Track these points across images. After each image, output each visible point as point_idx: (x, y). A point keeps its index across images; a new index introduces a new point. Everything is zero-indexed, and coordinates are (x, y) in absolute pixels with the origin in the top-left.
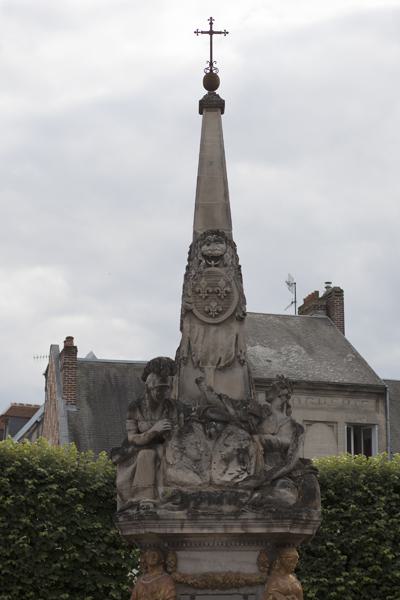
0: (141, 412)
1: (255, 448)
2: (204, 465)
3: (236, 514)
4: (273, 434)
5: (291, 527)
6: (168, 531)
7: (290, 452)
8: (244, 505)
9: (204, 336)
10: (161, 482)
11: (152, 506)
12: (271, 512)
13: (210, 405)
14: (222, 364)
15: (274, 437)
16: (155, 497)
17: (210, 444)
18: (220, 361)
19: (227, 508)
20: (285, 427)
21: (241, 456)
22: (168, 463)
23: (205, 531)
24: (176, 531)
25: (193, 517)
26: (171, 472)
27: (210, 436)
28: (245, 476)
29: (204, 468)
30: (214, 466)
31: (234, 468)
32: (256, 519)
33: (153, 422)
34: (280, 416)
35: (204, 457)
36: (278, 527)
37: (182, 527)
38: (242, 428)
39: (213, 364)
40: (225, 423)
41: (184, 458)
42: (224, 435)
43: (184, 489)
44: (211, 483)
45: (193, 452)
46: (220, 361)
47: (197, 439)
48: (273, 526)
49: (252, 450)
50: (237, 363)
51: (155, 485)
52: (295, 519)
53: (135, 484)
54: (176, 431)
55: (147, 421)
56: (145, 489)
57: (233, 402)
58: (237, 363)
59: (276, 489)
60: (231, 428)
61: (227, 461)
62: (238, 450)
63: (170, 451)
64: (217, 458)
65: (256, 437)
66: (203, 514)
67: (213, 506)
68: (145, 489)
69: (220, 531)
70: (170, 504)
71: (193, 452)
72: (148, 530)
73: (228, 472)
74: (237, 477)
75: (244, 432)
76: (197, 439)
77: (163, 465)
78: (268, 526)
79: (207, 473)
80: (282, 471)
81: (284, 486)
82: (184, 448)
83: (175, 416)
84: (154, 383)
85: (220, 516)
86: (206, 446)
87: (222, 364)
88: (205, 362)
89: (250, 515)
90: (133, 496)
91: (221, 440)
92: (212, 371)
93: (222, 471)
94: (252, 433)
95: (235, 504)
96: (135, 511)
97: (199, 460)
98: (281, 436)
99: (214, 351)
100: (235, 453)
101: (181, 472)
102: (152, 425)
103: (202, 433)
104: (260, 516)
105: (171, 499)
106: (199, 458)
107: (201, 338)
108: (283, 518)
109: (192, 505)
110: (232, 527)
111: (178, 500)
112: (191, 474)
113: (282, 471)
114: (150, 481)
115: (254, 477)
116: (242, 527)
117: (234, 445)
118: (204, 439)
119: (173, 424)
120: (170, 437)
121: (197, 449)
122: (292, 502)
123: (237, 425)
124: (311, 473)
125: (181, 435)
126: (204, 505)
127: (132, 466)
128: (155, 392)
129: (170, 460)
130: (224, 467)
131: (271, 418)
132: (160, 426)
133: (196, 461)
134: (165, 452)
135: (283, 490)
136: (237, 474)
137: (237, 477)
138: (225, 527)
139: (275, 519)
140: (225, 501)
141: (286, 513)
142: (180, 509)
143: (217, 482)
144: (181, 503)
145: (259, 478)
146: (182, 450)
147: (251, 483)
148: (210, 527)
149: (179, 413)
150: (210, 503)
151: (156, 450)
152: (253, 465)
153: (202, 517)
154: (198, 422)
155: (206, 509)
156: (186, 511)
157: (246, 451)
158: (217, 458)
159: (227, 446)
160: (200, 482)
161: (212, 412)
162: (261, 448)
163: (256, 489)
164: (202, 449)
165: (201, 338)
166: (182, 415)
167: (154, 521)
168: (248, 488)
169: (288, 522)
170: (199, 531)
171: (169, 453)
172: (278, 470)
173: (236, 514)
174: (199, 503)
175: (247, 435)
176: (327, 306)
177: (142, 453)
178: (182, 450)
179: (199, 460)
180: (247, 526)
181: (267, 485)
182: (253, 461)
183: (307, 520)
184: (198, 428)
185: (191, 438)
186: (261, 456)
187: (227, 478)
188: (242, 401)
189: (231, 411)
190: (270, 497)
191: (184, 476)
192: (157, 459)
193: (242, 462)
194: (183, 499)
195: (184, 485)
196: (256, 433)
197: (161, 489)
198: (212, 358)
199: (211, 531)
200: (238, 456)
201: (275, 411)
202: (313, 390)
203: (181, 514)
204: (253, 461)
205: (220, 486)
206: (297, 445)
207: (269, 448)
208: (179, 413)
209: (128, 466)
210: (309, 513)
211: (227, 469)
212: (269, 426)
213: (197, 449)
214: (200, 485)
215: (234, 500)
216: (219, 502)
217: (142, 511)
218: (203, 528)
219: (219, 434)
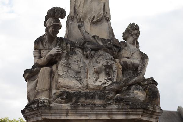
0: (43, 44)
1: (117, 66)
2: (83, 75)
3: (104, 106)
4: (128, 58)
5: (142, 115)
6: (58, 117)
7: (139, 69)
8: (110, 100)
9: (84, 5)
10: (54, 87)
11: (47, 102)
12: (128, 104)
13: (86, 41)
14: (95, 20)
15: (129, 60)
16: (50, 97)
17: (87, 62)
18: (94, 18)
19: (98, 102)
20: (135, 54)
21: (107, 70)
22: (59, 75)
23: (83, 118)
24: (63, 118)
25: (75, 108)
26: (61, 80)
27: (87, 57)
28: (110, 82)
29: (83, 78)
30: (89, 76)
31: (103, 78)
32: (119, 109)
33: (50, 49)
34: (132, 47)
35: (83, 70)
36: (133, 114)
37: (67, 115)
38: (108, 52)
39: (89, 20)
40: (96, 50)
41: (69, 71)
42: (96, 57)
43: (70, 91)
44: (87, 87)
45: (75, 67)
46: (94, 18)
47: (78, 58)
48: (129, 114)
49: (114, 67)
50: (104, 20)
51: (50, 89)
52: (145, 109)
53: (37, 89)
54: (65, 54)
55: (46, 49)
56: (43, 91)
57: (103, 40)
58: (104, 20)
59: (131, 91)
60: (100, 52)
61: (98, 73)
62: (105, 66)
63: (60, 68)
64: (91, 71)
65: (117, 60)
66: (82, 106)
67: (88, 101)
68: (43, 91)
69: (93, 117)
70: (59, 99)
71: (75, 67)
72: (44, 117)
73: (99, 80)
74: (105, 83)
75: (109, 55)
76: (78, 58)
77: (56, 76)
78: (126, 115)
79: (85, 80)
80: (134, 79)
81: (136, 89)
82: (70, 64)
83: (64, 45)
84: (50, 23)
85: (93, 107)
86: (84, 63)
87: (95, 20)
88: (84, 19)
89: (114, 106)
90: (35, 97)
91: (94, 59)
92: (89, 24)
93: (95, 79)
94: (115, 57)
95: (104, 99)
96: (36, 106)
97: (80, 72)
98: (133, 59)
99: (90, 13)
100: (104, 68)
101: (67, 79)
102: (49, 52)
103: (81, 55)
104: (121, 107)
105: (61, 95)
106: (79, 70)
107: (82, 5)
108: (137, 108)
109: (74, 100)
110: (101, 115)
111: (65, 96)
112: (74, 81)
113: (134, 79)
114: (47, 87)
115: (116, 83)
116: (109, 115)
117: (102, 62)
118: (83, 59)
119: (63, 50)
120: (60, 59)
121: (78, 65)
122: (142, 99)
123: (104, 50)
124: (152, 83)
125: (68, 56)
126: (82, 100)
127: (36, 80)
128: (51, 28)
129: (60, 73)
130: (96, 77)
131: (127, 48)
132: (54, 51)
133: (78, 73)
134: (57, 68)
135: (136, 92)
136: (105, 81)
137: (105, 83)
138: (97, 115)
139: (130, 109)
140: (97, 97)
141: (139, 105)
142: (66, 103)
143: (91, 87)
144: (67, 98)
145: (119, 83)
146: (68, 65)
147: (114, 87)
148: (86, 115)
149: (67, 44)
150: (86, 99)
151: (51, 68)
152: (115, 77)
153: (80, 108)
154: (79, 48)
155: (84, 102)
156: (70, 104)
157: (110, 67)
158: (91, 71)
159: (97, 63)
160: (80, 86)
161: (88, 44)
162: (121, 67)
163: (117, 92)
164: (81, 65)
165: (82, 5)
166: (69, 45)
167: (48, 111)
168: (112, 90)
169: (140, 111)
170: (79, 118)
171: (60, 68)
172: (132, 78)
173: (104, 106)
174: (79, 98)
175: (111, 57)
176: (133, 31)
177: (42, 69)
178: (68, 65)
179: (80, 72)
180: (112, 114)
181: (125, 90)
182: (115, 74)
183: (152, 111)
184: (79, 51)
185: (75, 58)
186: (120, 72)
187: (98, 84)
188: (108, 39)
189: (101, 44)
190: (127, 96)
191: (69, 82)
192: (52, 73)
193: (108, 74)
194: (67, 96)
195: (69, 88)
196: (117, 58)
197: (54, 91)
198: (89, 16)
199: (87, 118)
200: (105, 69)
201: (129, 44)
202: (74, 115)
203: (66, 106)
204: (115, 74)
205: (93, 89)
206: (144, 65)
207: (126, 68)
208: (67, 44)
209: (34, 80)
210: (153, 107)
211: (98, 78)
212: (125, 53)
213: (78, 65)
214: (80, 88)
215: (103, 96)
216: (93, 97)
217: (40, 105)
218: (81, 115)
219: (92, 57)
